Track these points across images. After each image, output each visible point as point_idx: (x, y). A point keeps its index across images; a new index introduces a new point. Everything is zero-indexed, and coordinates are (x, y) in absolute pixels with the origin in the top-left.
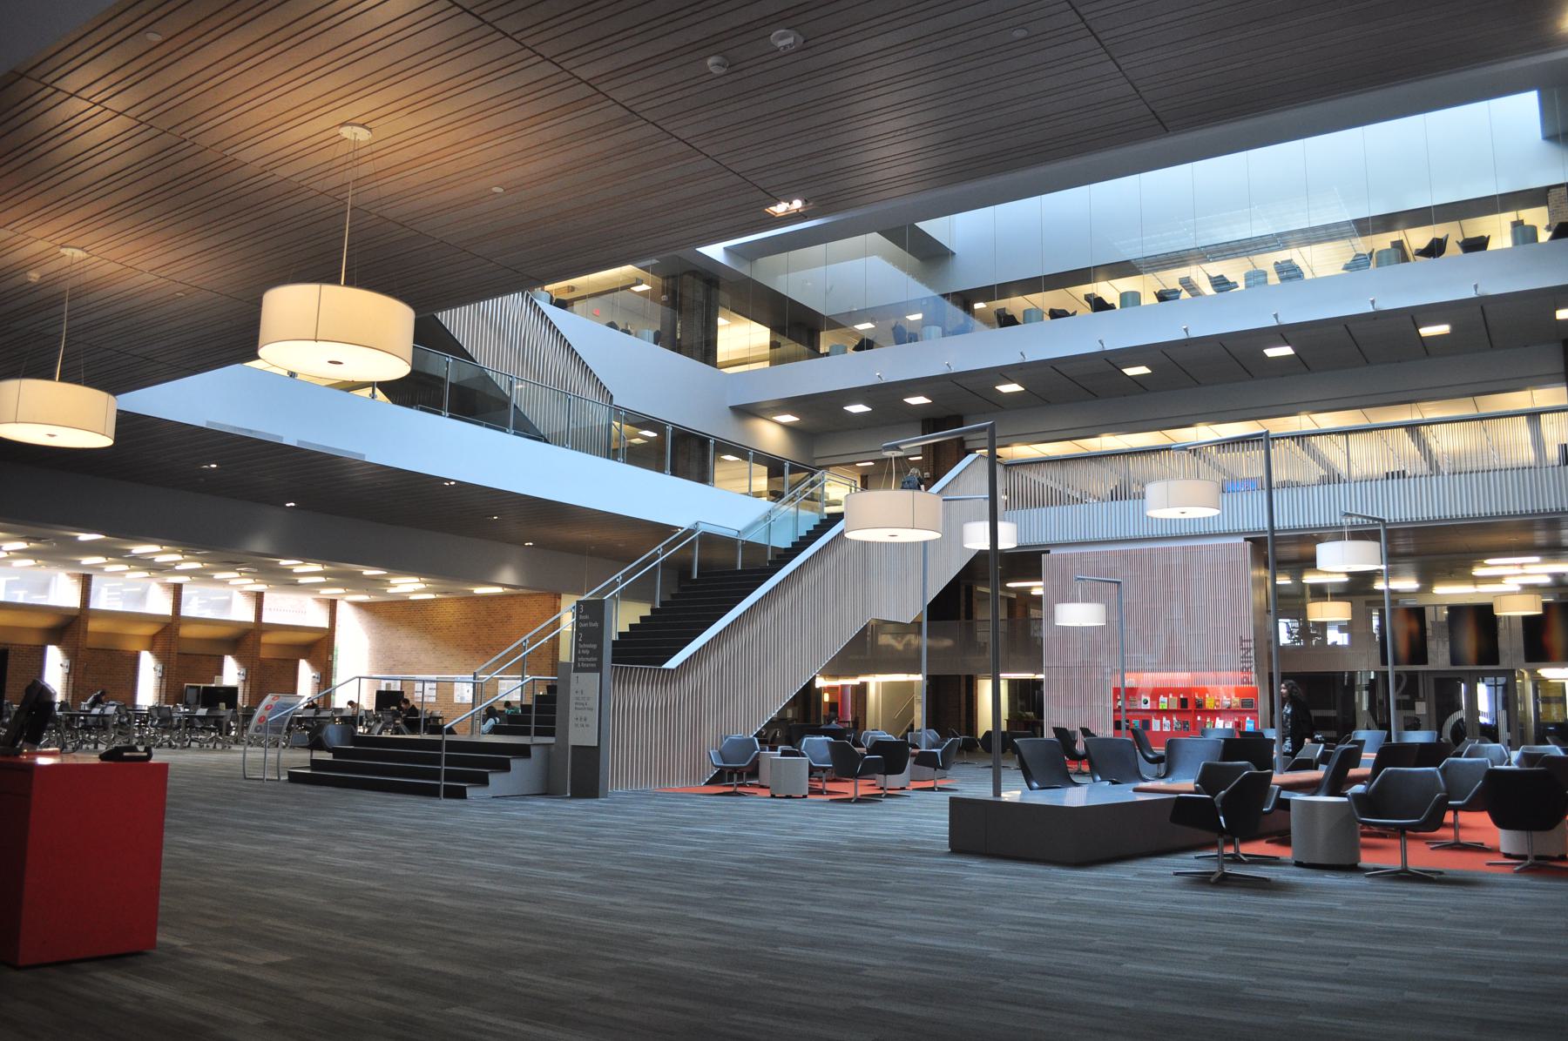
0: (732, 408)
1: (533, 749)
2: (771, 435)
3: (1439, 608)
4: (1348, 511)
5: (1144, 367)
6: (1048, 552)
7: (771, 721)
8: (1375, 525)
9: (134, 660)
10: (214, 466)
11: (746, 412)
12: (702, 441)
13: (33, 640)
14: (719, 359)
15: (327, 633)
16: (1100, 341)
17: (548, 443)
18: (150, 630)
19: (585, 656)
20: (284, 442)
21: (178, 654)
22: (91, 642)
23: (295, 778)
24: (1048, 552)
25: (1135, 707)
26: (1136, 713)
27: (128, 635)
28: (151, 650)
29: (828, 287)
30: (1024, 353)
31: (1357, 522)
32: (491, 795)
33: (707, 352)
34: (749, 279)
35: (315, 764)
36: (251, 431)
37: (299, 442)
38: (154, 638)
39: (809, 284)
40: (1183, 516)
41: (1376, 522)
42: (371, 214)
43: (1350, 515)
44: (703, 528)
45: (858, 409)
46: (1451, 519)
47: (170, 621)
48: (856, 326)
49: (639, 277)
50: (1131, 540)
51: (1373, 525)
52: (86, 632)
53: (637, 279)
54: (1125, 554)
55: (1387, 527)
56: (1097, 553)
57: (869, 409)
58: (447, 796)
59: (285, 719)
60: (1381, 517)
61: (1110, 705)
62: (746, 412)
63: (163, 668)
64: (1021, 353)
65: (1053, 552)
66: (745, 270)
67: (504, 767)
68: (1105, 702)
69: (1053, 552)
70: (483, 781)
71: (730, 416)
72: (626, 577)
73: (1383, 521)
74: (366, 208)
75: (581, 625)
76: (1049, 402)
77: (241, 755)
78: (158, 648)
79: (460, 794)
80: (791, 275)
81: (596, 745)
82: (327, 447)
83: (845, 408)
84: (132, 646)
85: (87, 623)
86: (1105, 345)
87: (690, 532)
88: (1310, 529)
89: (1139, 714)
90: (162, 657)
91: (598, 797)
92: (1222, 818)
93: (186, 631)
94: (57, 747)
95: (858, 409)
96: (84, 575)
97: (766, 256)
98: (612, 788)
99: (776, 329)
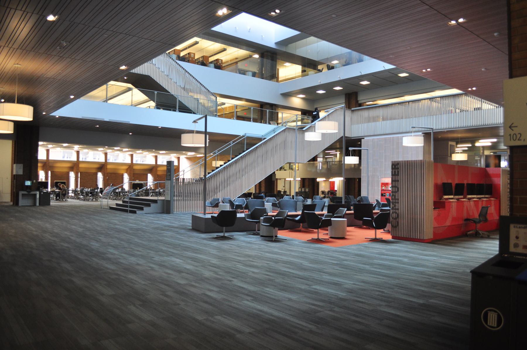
0: (281, 94)
1: (158, 201)
2: (297, 101)
3: (291, 164)
4: (413, 126)
5: (339, 87)
6: (364, 138)
7: (244, 194)
8: (429, 130)
9: (122, 175)
10: (98, 126)
11: (287, 95)
12: (273, 107)
13: (94, 171)
14: (280, 79)
15: (177, 167)
16: (383, 67)
17: (195, 114)
18: (125, 167)
19: (168, 176)
20: (105, 120)
21: (133, 174)
22: (109, 171)
23: (112, 208)
24: (364, 138)
25: (387, 189)
26: (388, 191)
27: (120, 169)
28: (127, 173)
29: (318, 51)
30: (385, 67)
31: (421, 130)
32: (144, 213)
33: (273, 76)
34: (286, 52)
35: (117, 205)
36: (95, 118)
37: (109, 120)
38: (127, 169)
39: (309, 51)
40: (327, 132)
41: (430, 129)
42: (55, 79)
43: (414, 127)
44: (248, 135)
45: (321, 92)
46: (495, 124)
47: (130, 165)
48: (332, 62)
49: (250, 54)
50: (377, 135)
51: (429, 130)
52: (107, 168)
53: (250, 55)
54: (385, 139)
55: (434, 131)
56: (377, 138)
57: (325, 92)
58: (130, 212)
59: (109, 193)
60: (431, 127)
61: (380, 188)
62: (287, 95)
63: (130, 178)
64: (360, 72)
65: (365, 138)
66: (283, 49)
67: (149, 205)
68: (378, 187)
69: (365, 138)
70: (142, 209)
71: (281, 96)
72: (218, 151)
73: (432, 128)
74: (52, 77)
75: (168, 168)
76: (413, 81)
77: (107, 202)
78: (128, 172)
79: (135, 212)
80: (318, 43)
81: (170, 200)
82: (117, 121)
83: (317, 92)
84: (121, 172)
85: (107, 166)
86: (341, 78)
87: (243, 136)
88: (443, 129)
89: (389, 191)
90: (129, 175)
91: (170, 214)
92: (374, 223)
93: (135, 167)
94: (345, 202)
95: (321, 92)
96: (105, 153)
97: (290, 44)
98: (208, 211)
99: (303, 66)
